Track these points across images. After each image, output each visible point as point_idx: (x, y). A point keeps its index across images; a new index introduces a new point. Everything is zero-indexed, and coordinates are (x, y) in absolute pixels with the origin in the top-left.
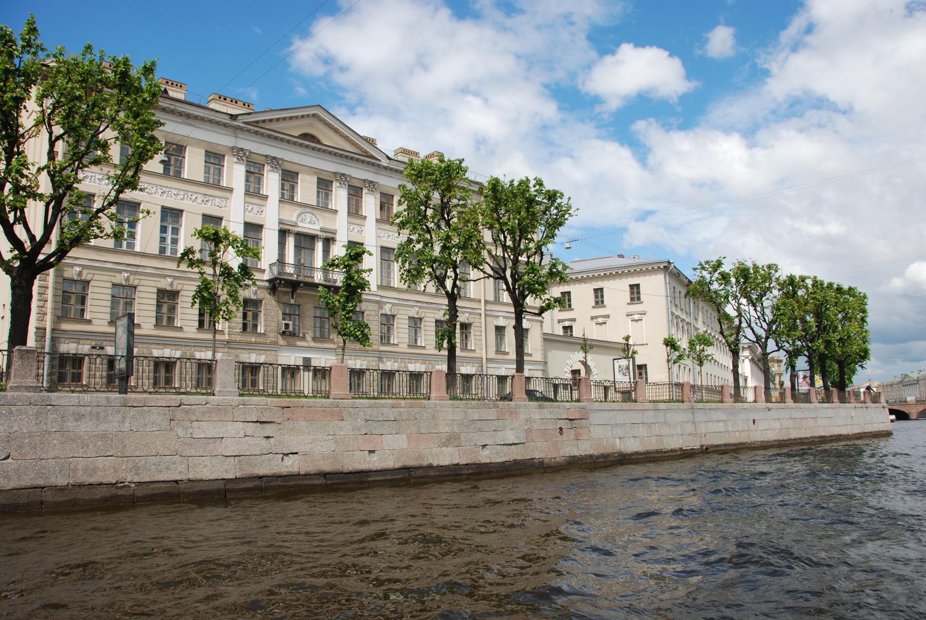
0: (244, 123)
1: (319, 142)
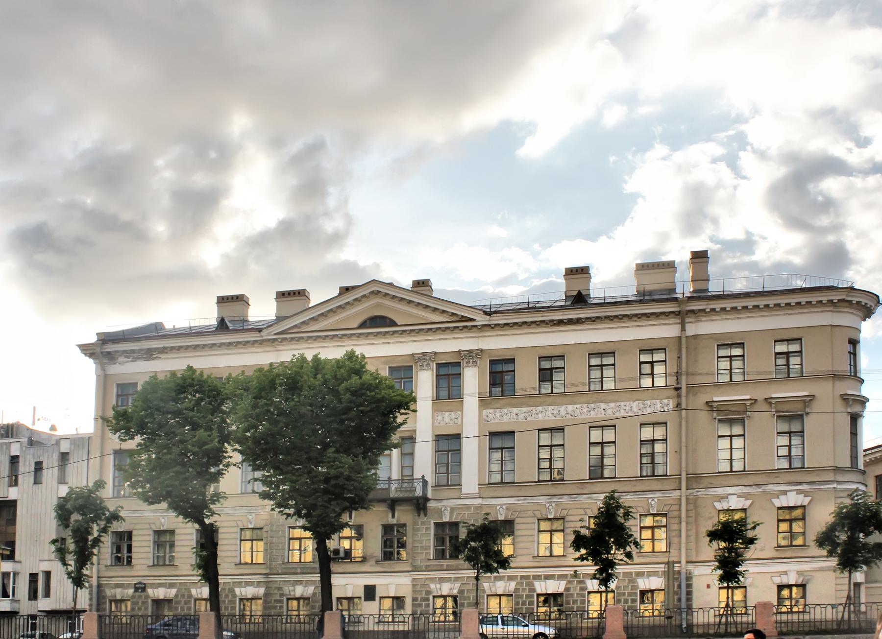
0: (275, 334)
1: (473, 320)
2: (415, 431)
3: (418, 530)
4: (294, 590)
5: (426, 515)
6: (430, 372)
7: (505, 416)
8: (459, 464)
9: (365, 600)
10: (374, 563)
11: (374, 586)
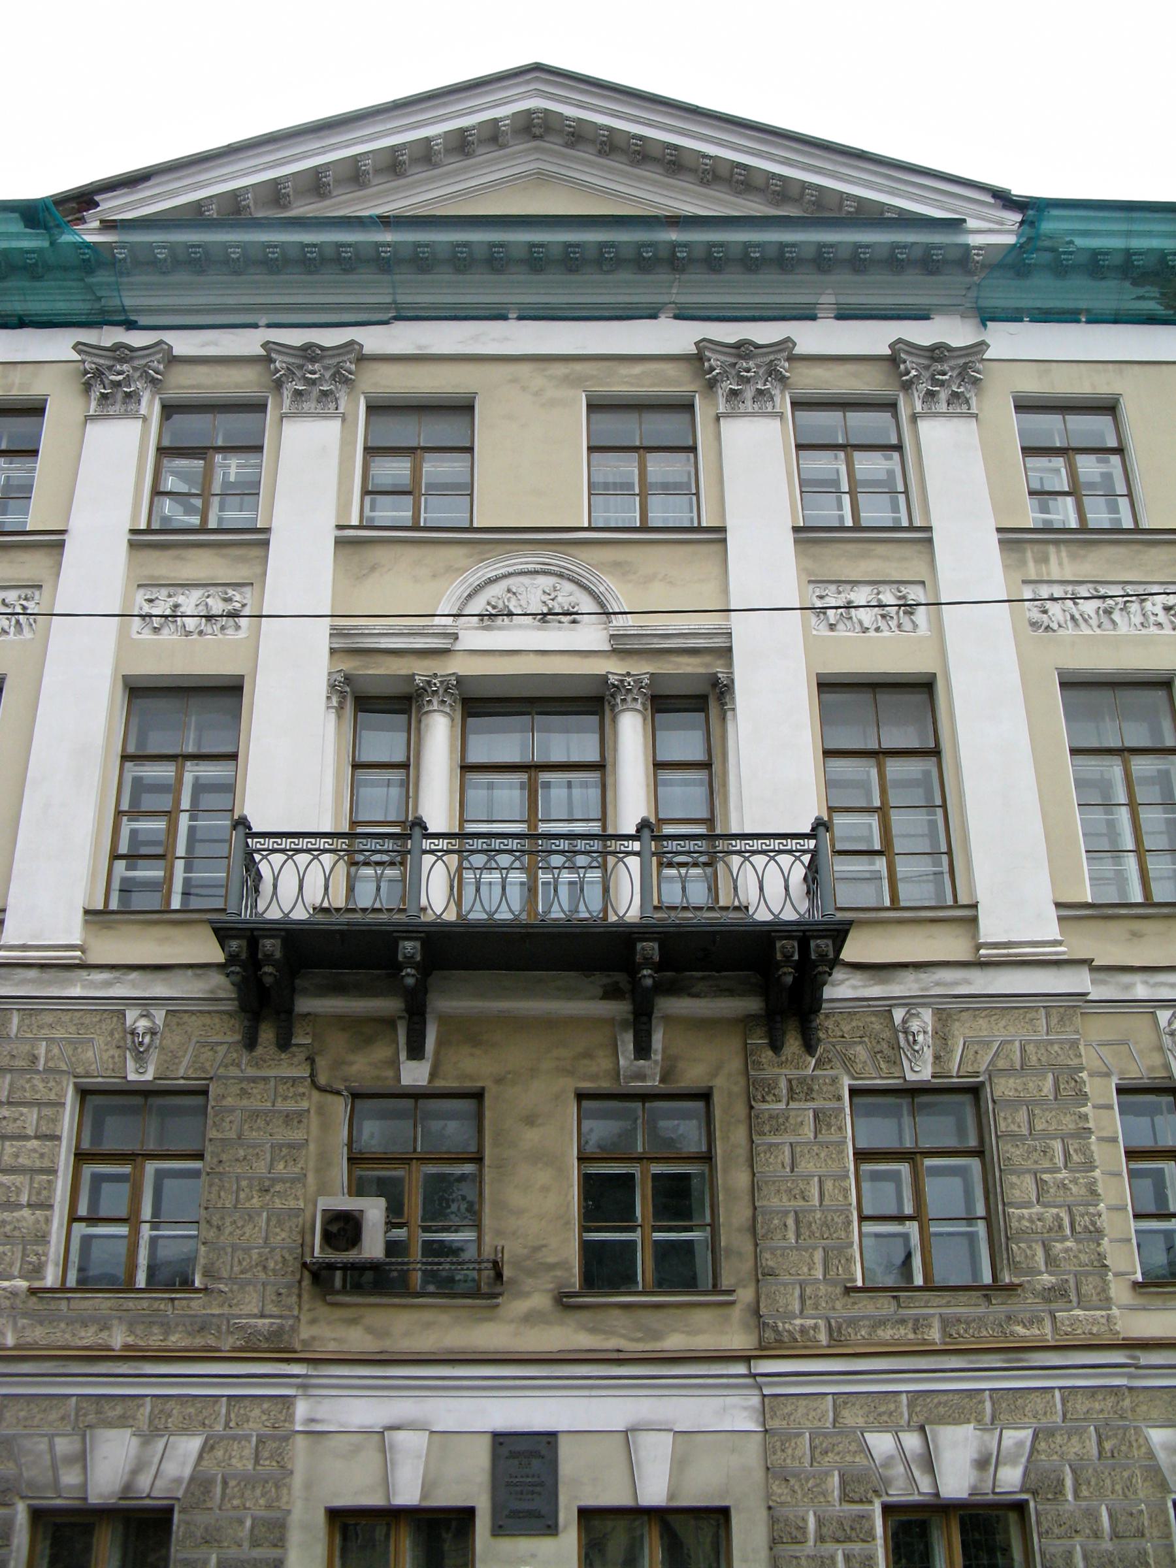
2: (726, 652)
3: (779, 1124)
4: (82, 1459)
5: (809, 1047)
6: (331, 429)
7: (419, 596)
8: (940, 803)
9: (498, 1530)
10: (540, 1301)
11: (550, 1438)
